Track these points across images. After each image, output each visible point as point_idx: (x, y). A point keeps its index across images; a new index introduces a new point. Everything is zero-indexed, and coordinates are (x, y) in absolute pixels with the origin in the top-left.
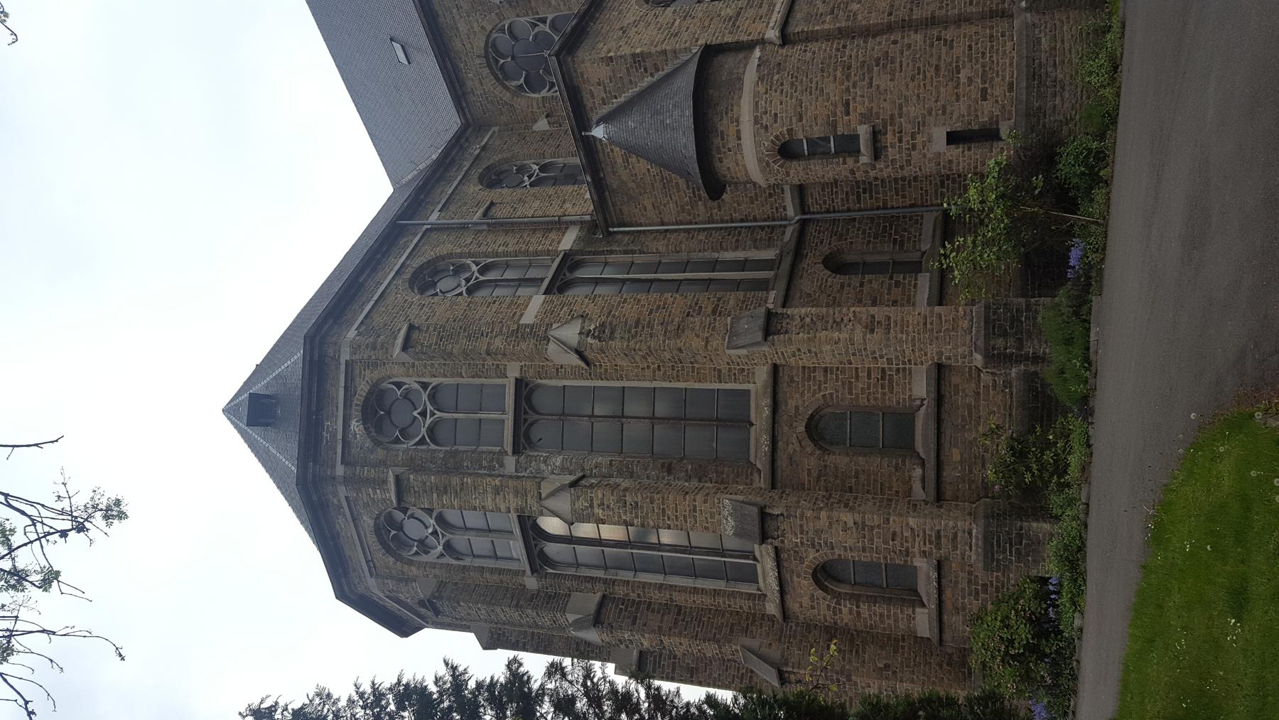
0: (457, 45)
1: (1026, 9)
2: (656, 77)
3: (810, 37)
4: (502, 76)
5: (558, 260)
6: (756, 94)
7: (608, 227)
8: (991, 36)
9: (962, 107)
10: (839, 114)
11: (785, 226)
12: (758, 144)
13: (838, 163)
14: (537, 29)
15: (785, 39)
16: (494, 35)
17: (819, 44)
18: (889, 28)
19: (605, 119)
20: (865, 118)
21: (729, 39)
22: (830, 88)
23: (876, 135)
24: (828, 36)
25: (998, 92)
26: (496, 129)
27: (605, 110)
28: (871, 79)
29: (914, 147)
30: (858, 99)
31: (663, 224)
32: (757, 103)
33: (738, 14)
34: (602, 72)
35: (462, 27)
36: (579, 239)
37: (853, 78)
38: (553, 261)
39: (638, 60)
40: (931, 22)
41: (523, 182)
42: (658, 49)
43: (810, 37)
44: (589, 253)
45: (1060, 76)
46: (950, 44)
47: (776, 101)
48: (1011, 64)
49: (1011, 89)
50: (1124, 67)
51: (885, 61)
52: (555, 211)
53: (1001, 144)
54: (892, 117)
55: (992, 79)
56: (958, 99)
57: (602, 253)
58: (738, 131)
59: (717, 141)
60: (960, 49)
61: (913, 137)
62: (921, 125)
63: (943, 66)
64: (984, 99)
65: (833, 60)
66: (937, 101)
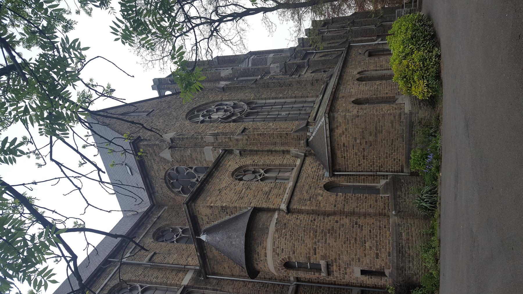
0: (153, 173)
1: (395, 215)
2: (232, 216)
3: (300, 212)
4: (171, 187)
5: (181, 290)
6: (274, 238)
7: (206, 274)
8: (380, 227)
9: (367, 260)
10: (311, 254)
11: (289, 286)
12: (274, 261)
13: (311, 274)
14: (188, 171)
15: (289, 210)
16: (169, 171)
17: (303, 216)
18: (334, 214)
19: (208, 231)
20: (323, 257)
21: (264, 205)
22: (307, 241)
23: (328, 266)
24: (308, 213)
25: (383, 256)
26: (166, 207)
27: (208, 226)
28: (326, 239)
29: (346, 273)
30: (320, 248)
31: (233, 276)
32: (274, 242)
33: (270, 191)
34: (208, 211)
35: (155, 167)
36: (192, 279)
37: (318, 238)
38: (178, 289)
39: (224, 209)
40: (352, 214)
41: (173, 237)
42: (233, 205)
43: (300, 212)
44: (196, 288)
45: (412, 254)
46: (361, 227)
47: (283, 243)
48: (389, 243)
49: (389, 256)
50: (441, 261)
51: (332, 231)
52: (183, 262)
53: (386, 278)
54: (335, 259)
55: (380, 249)
56: (365, 256)
57: (202, 289)
58: (266, 253)
59: (256, 256)
60: (366, 231)
61: (345, 269)
62: (349, 265)
63: (358, 239)
64: (377, 258)
65: (309, 227)
66: (356, 255)
